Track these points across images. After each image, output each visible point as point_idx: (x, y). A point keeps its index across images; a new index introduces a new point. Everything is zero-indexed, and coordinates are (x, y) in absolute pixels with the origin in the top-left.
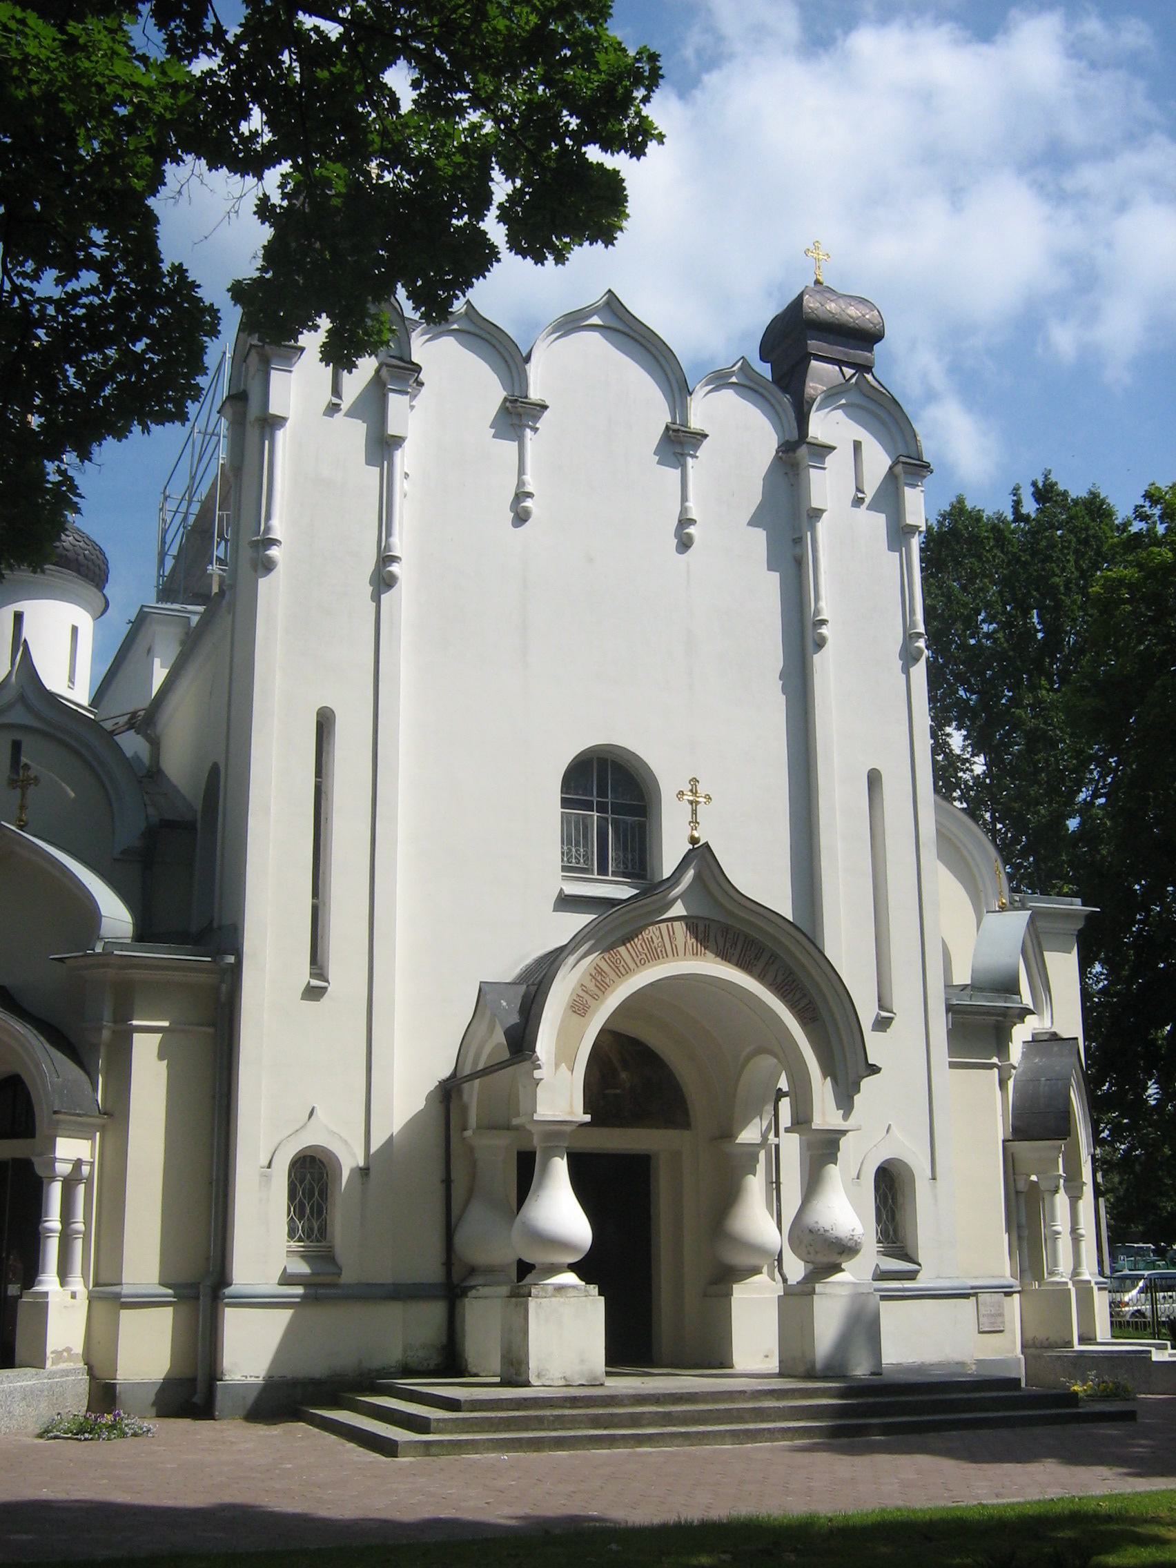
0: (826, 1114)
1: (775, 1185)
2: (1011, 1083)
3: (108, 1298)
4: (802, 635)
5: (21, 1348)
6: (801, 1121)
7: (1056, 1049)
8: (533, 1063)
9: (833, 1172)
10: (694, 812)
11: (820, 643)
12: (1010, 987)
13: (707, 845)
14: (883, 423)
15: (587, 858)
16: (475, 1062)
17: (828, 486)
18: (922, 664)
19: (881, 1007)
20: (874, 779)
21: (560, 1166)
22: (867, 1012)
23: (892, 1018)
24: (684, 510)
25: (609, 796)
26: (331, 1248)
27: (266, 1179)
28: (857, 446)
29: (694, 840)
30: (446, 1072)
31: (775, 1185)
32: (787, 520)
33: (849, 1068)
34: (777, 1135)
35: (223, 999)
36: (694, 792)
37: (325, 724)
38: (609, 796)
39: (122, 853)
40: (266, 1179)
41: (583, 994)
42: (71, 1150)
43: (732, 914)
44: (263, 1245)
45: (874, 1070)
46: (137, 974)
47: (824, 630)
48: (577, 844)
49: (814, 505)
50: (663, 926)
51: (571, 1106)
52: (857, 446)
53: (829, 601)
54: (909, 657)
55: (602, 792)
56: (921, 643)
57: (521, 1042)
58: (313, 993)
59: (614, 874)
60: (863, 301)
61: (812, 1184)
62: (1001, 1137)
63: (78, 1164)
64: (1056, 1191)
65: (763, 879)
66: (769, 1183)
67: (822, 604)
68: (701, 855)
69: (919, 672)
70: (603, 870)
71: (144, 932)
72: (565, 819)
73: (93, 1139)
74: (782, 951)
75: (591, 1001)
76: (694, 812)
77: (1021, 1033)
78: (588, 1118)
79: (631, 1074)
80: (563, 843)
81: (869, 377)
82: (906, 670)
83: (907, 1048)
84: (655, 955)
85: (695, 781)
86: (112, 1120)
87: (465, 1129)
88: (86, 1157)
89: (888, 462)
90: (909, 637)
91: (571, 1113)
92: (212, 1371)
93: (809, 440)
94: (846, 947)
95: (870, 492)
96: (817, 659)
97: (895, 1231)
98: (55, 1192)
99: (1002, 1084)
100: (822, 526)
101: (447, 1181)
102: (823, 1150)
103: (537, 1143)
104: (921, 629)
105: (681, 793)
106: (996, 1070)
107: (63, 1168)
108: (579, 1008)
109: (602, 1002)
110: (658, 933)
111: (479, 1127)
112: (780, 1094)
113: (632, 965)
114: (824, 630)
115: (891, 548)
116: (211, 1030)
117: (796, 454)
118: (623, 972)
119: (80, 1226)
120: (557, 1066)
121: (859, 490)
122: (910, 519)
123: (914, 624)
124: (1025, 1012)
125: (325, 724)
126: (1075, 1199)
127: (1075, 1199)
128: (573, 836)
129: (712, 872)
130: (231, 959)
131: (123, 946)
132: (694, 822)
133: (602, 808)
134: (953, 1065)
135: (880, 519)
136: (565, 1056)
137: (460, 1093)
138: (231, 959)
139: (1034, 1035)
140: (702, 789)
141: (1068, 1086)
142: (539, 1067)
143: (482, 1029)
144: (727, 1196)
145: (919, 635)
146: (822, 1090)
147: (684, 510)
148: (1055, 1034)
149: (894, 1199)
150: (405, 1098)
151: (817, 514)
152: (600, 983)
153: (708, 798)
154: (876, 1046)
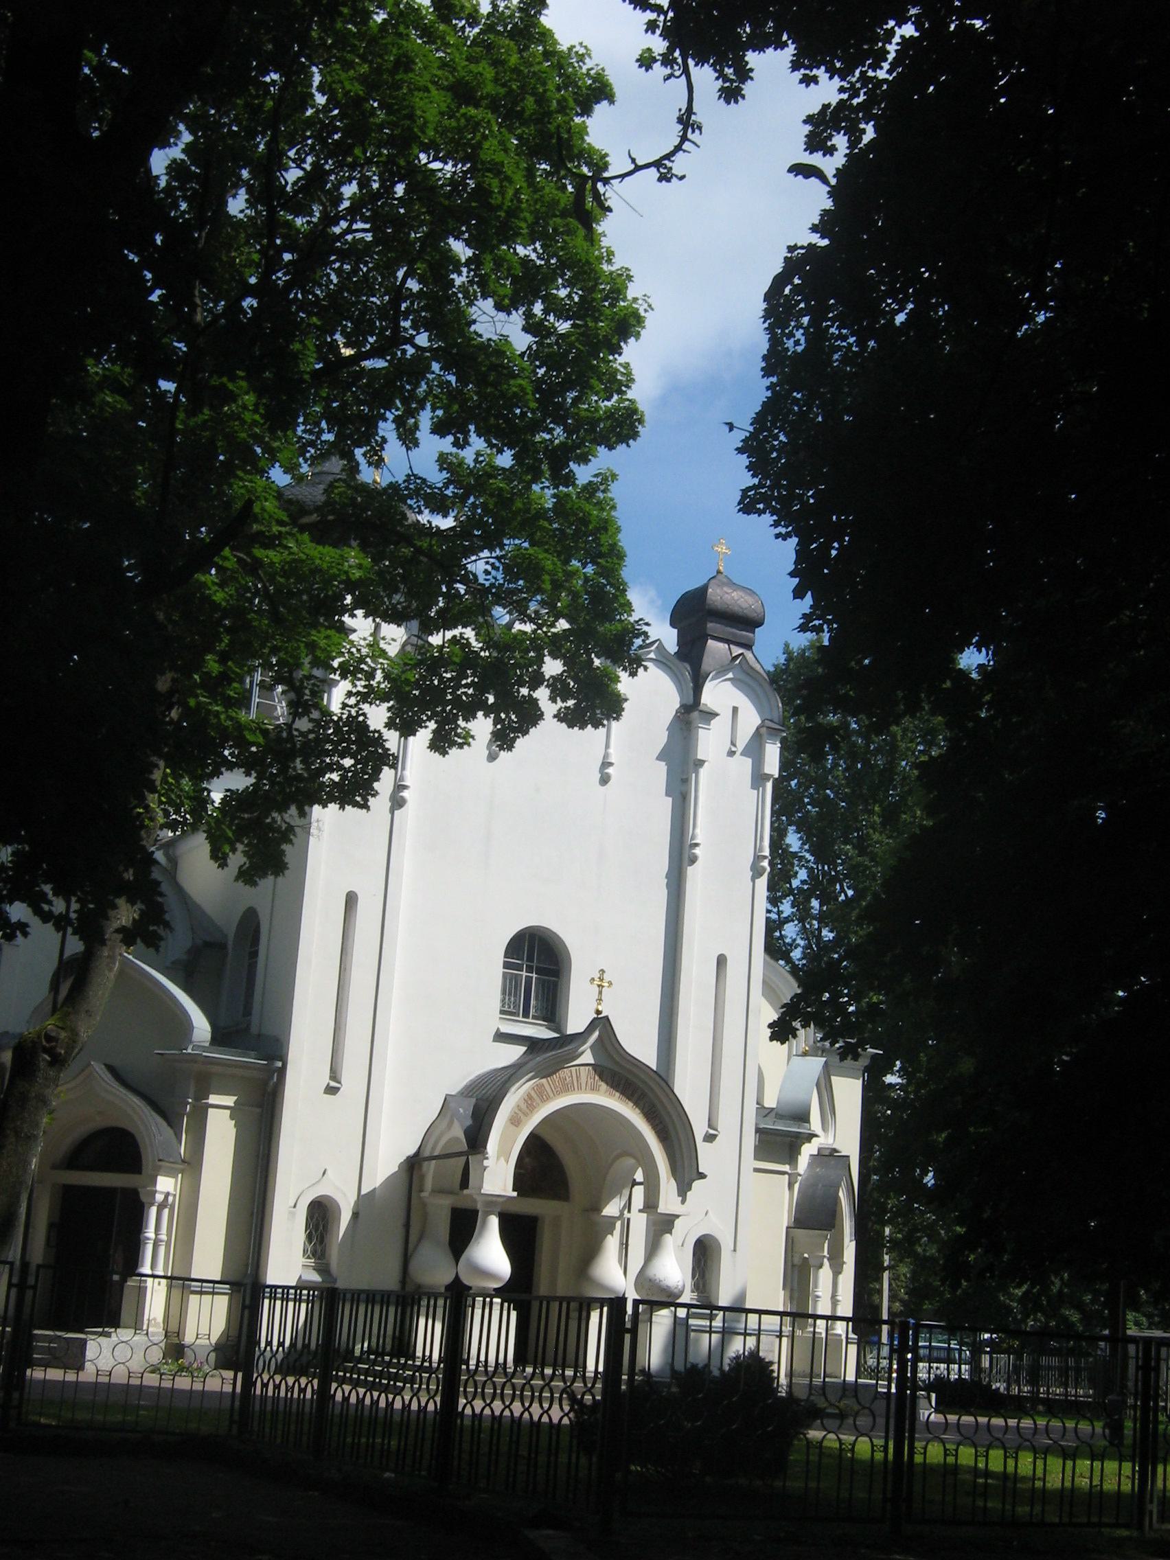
0: (668, 1201)
1: (625, 1245)
2: (797, 1186)
3: (181, 1283)
4: (681, 854)
5: (125, 1315)
6: (650, 1205)
9: (668, 1238)
10: (600, 993)
11: (693, 860)
12: (802, 1117)
13: (607, 1018)
14: (754, 690)
15: (516, 1006)
16: (433, 1149)
17: (711, 742)
18: (765, 878)
19: (710, 1126)
20: (721, 961)
21: (494, 1222)
22: (699, 1128)
23: (338, 1089)
24: (606, 755)
25: (537, 961)
26: (328, 1265)
27: (292, 1215)
28: (735, 710)
29: (598, 1012)
30: (411, 1151)
31: (625, 1245)
32: (681, 763)
33: (687, 1172)
34: (629, 1211)
35: (269, 1089)
36: (601, 979)
37: (351, 900)
38: (537, 961)
39: (173, 963)
40: (292, 1215)
42: (165, 1185)
43: (617, 1063)
44: (287, 1261)
45: (702, 1176)
46: (215, 1069)
47: (697, 851)
48: (510, 994)
49: (699, 757)
52: (735, 710)
53: (702, 830)
54: (757, 872)
55: (530, 959)
56: (765, 863)
57: (476, 1139)
58: (331, 1090)
59: (534, 1017)
60: (751, 592)
61: (653, 1248)
62: (785, 1224)
63: (167, 1194)
64: (821, 1266)
65: (640, 1044)
66: (621, 1244)
67: (698, 831)
68: (601, 1023)
69: (763, 882)
70: (526, 1015)
71: (220, 1038)
72: (504, 974)
73: (176, 1177)
74: (649, 1089)
76: (600, 993)
77: (808, 1150)
78: (515, 1194)
79: (541, 1165)
80: (504, 992)
81: (749, 655)
82: (753, 880)
83: (726, 1155)
84: (566, 1088)
85: (603, 971)
86: (192, 1166)
87: (422, 1191)
88: (172, 1191)
89: (758, 721)
90: (758, 858)
92: (253, 1340)
93: (701, 707)
94: (689, 1088)
95: (741, 745)
96: (690, 871)
97: (704, 1285)
98: (154, 1210)
99: (791, 1186)
100: (703, 772)
101: (407, 1226)
102: (662, 1225)
103: (479, 1206)
104: (767, 852)
105: (593, 979)
106: (787, 1176)
107: (159, 1198)
108: (515, 1121)
111: (433, 1191)
112: (635, 1183)
114: (697, 851)
115: (753, 787)
116: (258, 1110)
117: (691, 714)
118: (544, 1098)
119: (164, 1237)
120: (498, 1158)
121: (733, 744)
122: (767, 770)
123: (761, 849)
124: (811, 1136)
125: (351, 900)
126: (837, 1270)
127: (837, 1270)
128: (510, 986)
130: (279, 1064)
131: (204, 1049)
132: (600, 1000)
133: (529, 969)
134: (757, 1170)
135: (748, 763)
136: (504, 1152)
137: (420, 1167)
138: (279, 1064)
139: (819, 1149)
140: (607, 977)
141: (839, 1186)
143: (443, 1125)
144: (590, 1252)
145: (765, 857)
147: (606, 755)
148: (835, 1150)
149: (705, 1262)
150: (385, 1164)
151: (701, 763)
152: (530, 1104)
153: (610, 983)
154: (707, 1156)
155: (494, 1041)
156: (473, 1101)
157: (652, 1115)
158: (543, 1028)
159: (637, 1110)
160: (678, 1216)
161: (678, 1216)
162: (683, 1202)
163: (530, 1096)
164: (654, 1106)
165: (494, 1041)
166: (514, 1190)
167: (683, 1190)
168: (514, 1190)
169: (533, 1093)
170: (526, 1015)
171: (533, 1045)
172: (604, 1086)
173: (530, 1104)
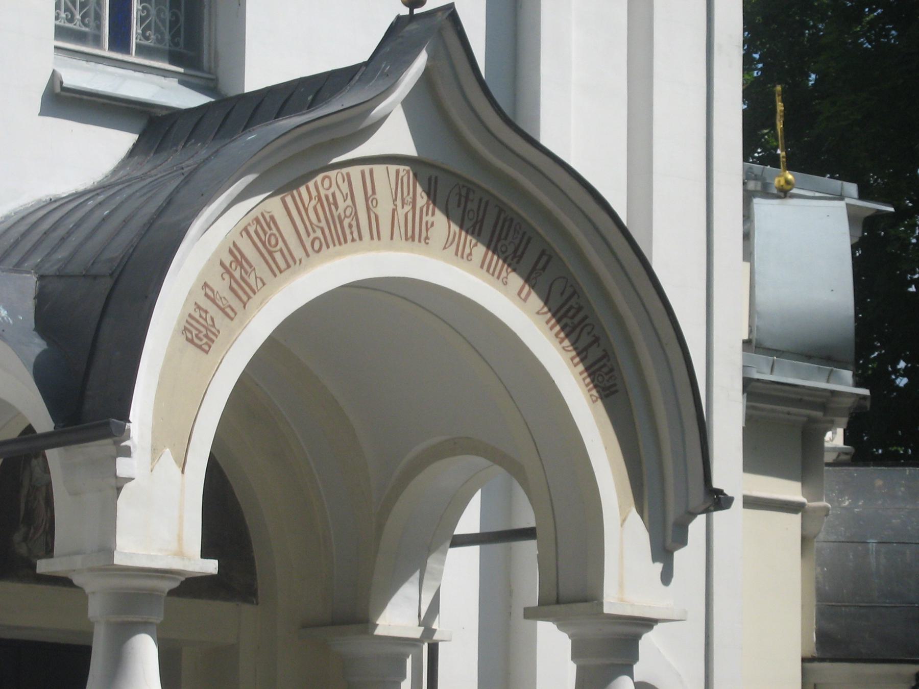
7: (879, 483)
8: (117, 443)
41: (206, 304)
50: (355, 172)
51: (180, 539)
59: (142, 50)
70: (120, 40)
75: (220, 321)
78: (211, 566)
84: (337, 233)
91: (180, 554)
108: (200, 334)
109: (243, 326)
110: (345, 188)
113: (298, 252)
118: (282, 264)
120: (156, 453)
129: (453, 67)
142: (127, 452)
146: (624, 535)
152: (239, 279)
155: (44, 112)
156: (30, 282)
157: (574, 318)
158: (173, 82)
159: (536, 302)
160: (648, 623)
161: (648, 623)
162: (667, 577)
163: (238, 256)
164: (576, 292)
165: (44, 112)
166: (206, 553)
167: (665, 544)
168: (206, 553)
169: (246, 247)
170: (120, 40)
171: (155, 127)
172: (441, 224)
173: (239, 279)
